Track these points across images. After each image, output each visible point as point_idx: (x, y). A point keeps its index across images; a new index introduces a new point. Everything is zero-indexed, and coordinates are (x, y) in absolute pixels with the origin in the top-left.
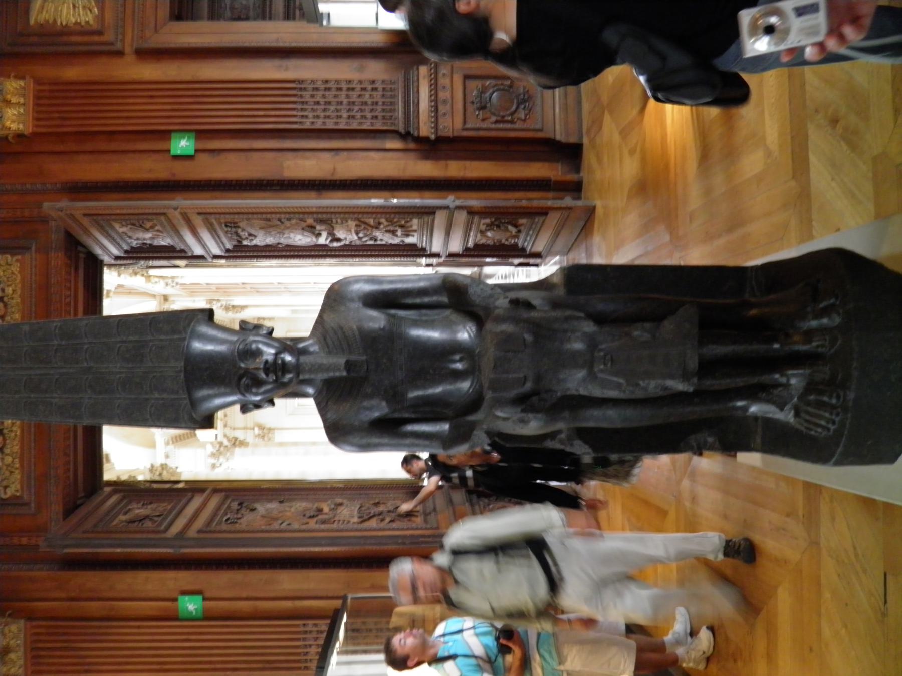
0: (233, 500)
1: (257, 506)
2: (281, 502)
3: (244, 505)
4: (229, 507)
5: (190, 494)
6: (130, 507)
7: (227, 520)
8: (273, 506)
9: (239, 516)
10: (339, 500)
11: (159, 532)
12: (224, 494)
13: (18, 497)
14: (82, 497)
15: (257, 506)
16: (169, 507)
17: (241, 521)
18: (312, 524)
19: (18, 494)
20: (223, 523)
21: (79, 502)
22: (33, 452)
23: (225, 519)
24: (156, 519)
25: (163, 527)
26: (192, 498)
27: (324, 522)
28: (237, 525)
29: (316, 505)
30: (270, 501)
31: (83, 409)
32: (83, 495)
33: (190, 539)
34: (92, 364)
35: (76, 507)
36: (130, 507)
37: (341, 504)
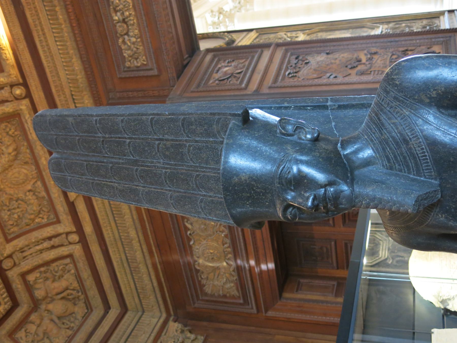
0: (292, 55)
1: (310, 58)
2: (328, 54)
3: (300, 58)
4: (289, 62)
5: (260, 50)
6: (219, 66)
7: (289, 74)
8: (322, 58)
9: (298, 70)
10: (374, 50)
11: (241, 89)
12: (284, 48)
13: (145, 65)
14: (187, 58)
15: (310, 58)
16: (247, 63)
17: (301, 73)
18: (354, 78)
19: (145, 63)
20: (286, 78)
21: (185, 62)
22: (148, 34)
23: (287, 73)
24: (238, 75)
25: (243, 85)
26: (262, 52)
27: (362, 73)
28: (296, 79)
29: (355, 56)
30: (319, 53)
31: (141, 195)
32: (187, 56)
33: (264, 94)
34: (138, 158)
35: (185, 66)
36: (219, 66)
37: (375, 53)
